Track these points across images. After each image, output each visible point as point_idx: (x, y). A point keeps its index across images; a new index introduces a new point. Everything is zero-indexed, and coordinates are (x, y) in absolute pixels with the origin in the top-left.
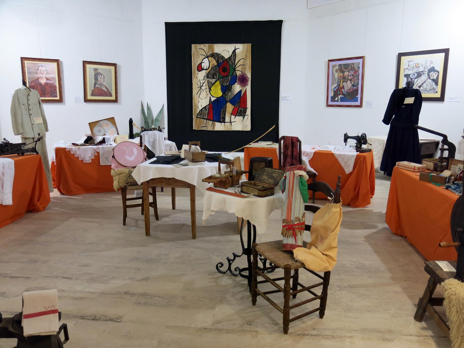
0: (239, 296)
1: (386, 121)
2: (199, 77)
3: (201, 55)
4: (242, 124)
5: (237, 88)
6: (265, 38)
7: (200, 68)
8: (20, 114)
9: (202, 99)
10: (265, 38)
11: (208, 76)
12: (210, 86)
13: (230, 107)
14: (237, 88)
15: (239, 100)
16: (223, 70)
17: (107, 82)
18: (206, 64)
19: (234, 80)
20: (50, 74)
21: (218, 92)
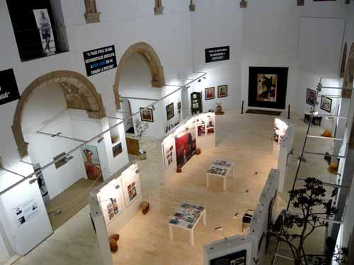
0: (283, 215)
1: (100, 95)
2: (260, 84)
3: (261, 78)
4: (273, 99)
5: (272, 88)
6: (282, 73)
7: (260, 81)
8: (141, 47)
9: (260, 91)
10: (282, 73)
11: (263, 84)
12: (263, 87)
13: (269, 94)
14: (272, 88)
15: (273, 91)
16: (268, 83)
17: (224, 91)
18: (262, 80)
19: (271, 85)
20: (206, 182)
21: (265, 89)
